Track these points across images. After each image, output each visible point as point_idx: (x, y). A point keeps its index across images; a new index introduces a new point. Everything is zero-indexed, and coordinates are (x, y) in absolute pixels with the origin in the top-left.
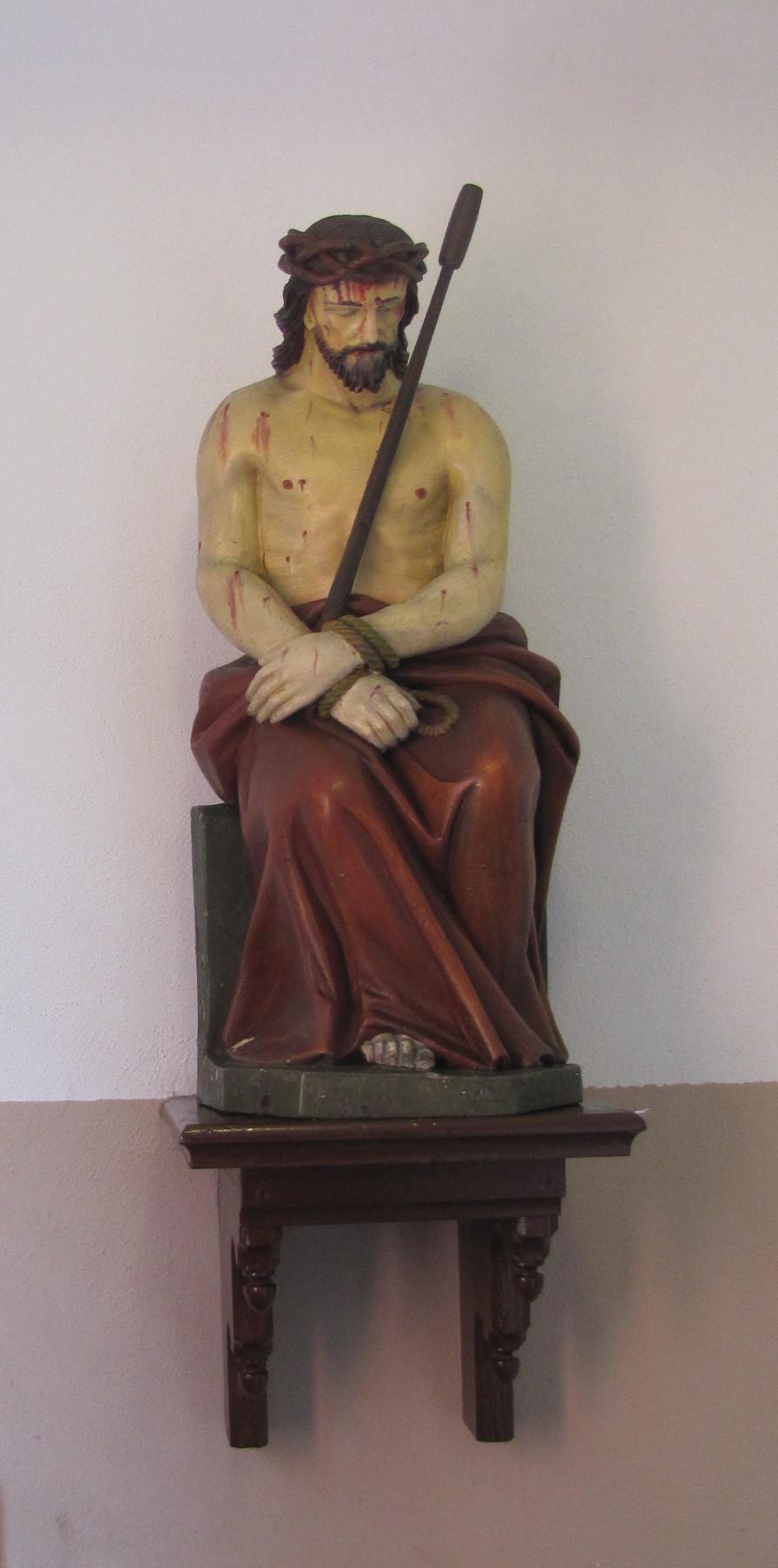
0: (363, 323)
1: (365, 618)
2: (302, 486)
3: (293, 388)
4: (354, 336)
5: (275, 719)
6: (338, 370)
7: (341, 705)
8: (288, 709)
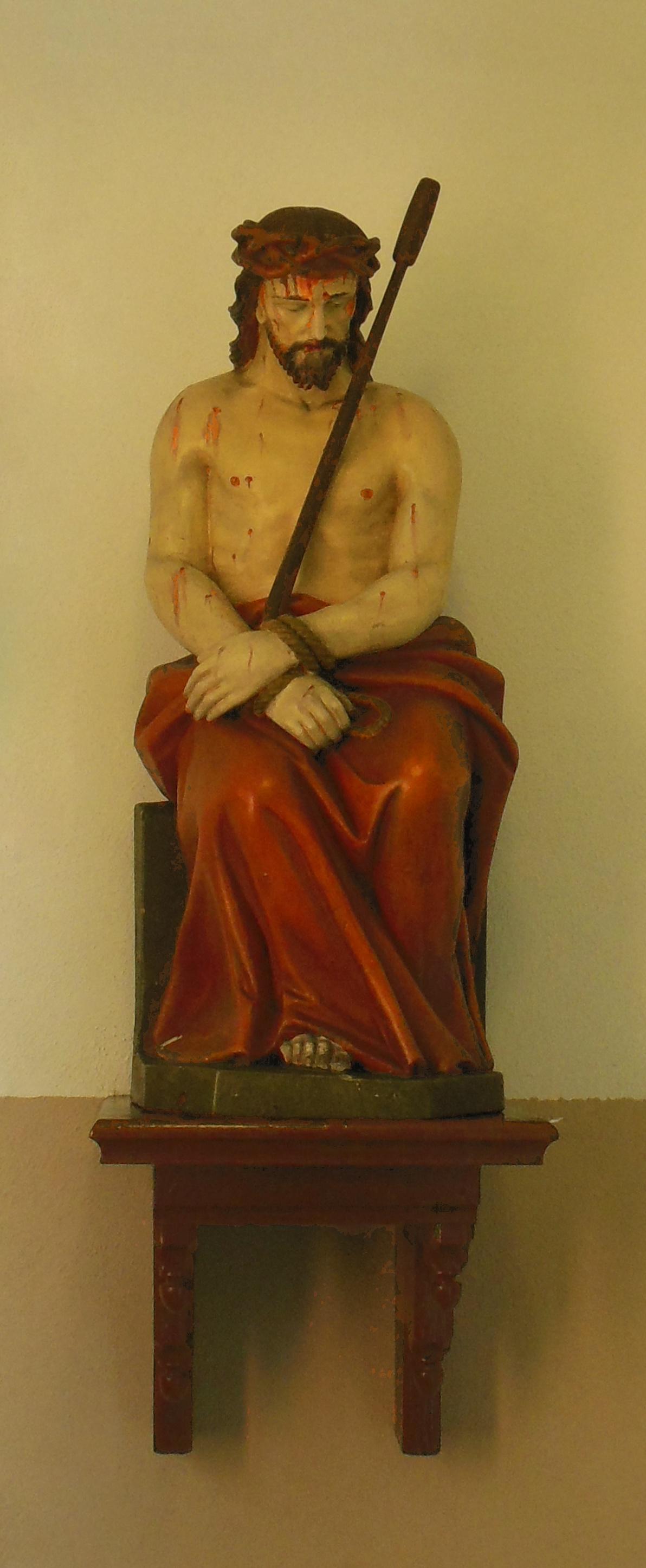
0: (310, 320)
1: (301, 618)
2: (249, 482)
3: (245, 384)
4: (302, 332)
5: (210, 717)
6: (288, 366)
7: (275, 704)
8: (223, 707)
